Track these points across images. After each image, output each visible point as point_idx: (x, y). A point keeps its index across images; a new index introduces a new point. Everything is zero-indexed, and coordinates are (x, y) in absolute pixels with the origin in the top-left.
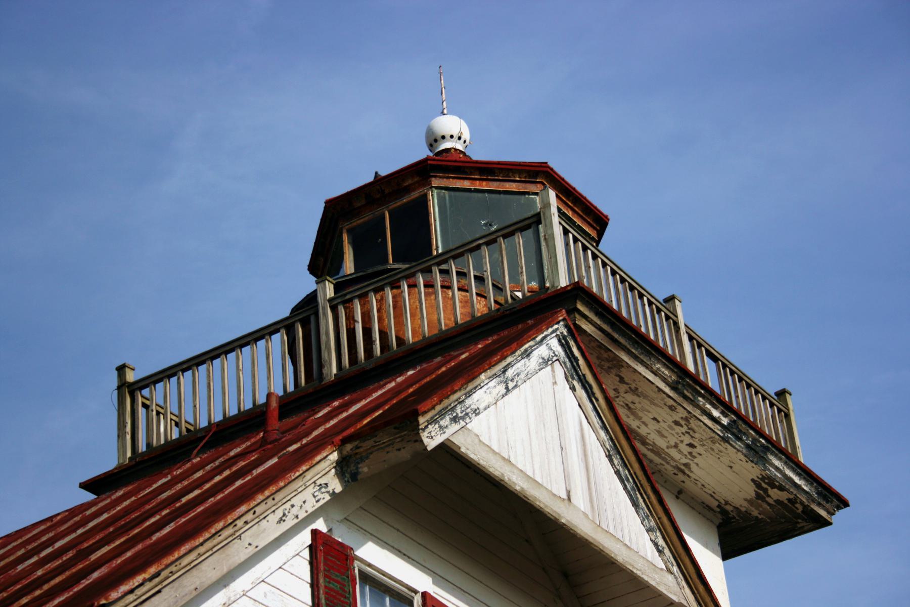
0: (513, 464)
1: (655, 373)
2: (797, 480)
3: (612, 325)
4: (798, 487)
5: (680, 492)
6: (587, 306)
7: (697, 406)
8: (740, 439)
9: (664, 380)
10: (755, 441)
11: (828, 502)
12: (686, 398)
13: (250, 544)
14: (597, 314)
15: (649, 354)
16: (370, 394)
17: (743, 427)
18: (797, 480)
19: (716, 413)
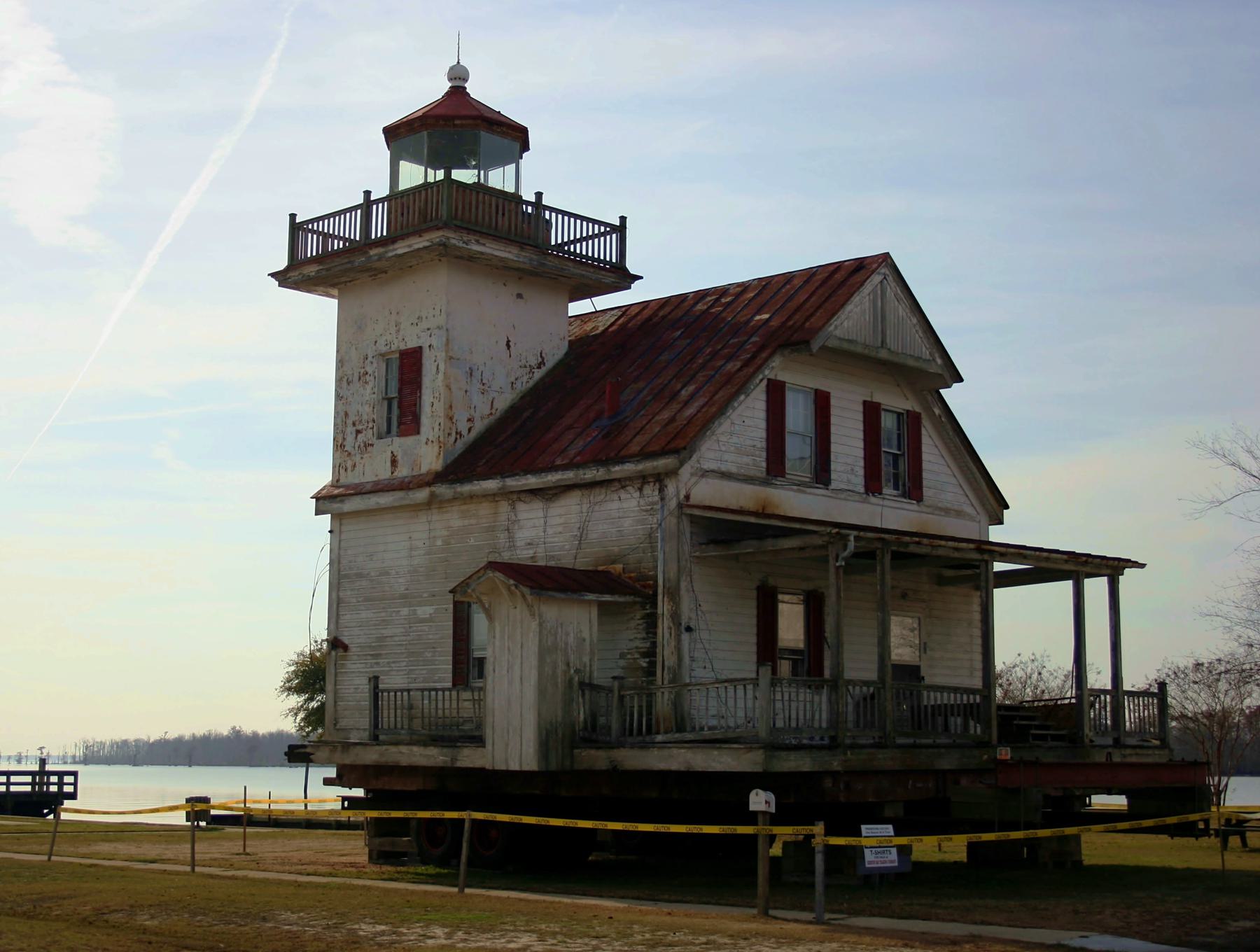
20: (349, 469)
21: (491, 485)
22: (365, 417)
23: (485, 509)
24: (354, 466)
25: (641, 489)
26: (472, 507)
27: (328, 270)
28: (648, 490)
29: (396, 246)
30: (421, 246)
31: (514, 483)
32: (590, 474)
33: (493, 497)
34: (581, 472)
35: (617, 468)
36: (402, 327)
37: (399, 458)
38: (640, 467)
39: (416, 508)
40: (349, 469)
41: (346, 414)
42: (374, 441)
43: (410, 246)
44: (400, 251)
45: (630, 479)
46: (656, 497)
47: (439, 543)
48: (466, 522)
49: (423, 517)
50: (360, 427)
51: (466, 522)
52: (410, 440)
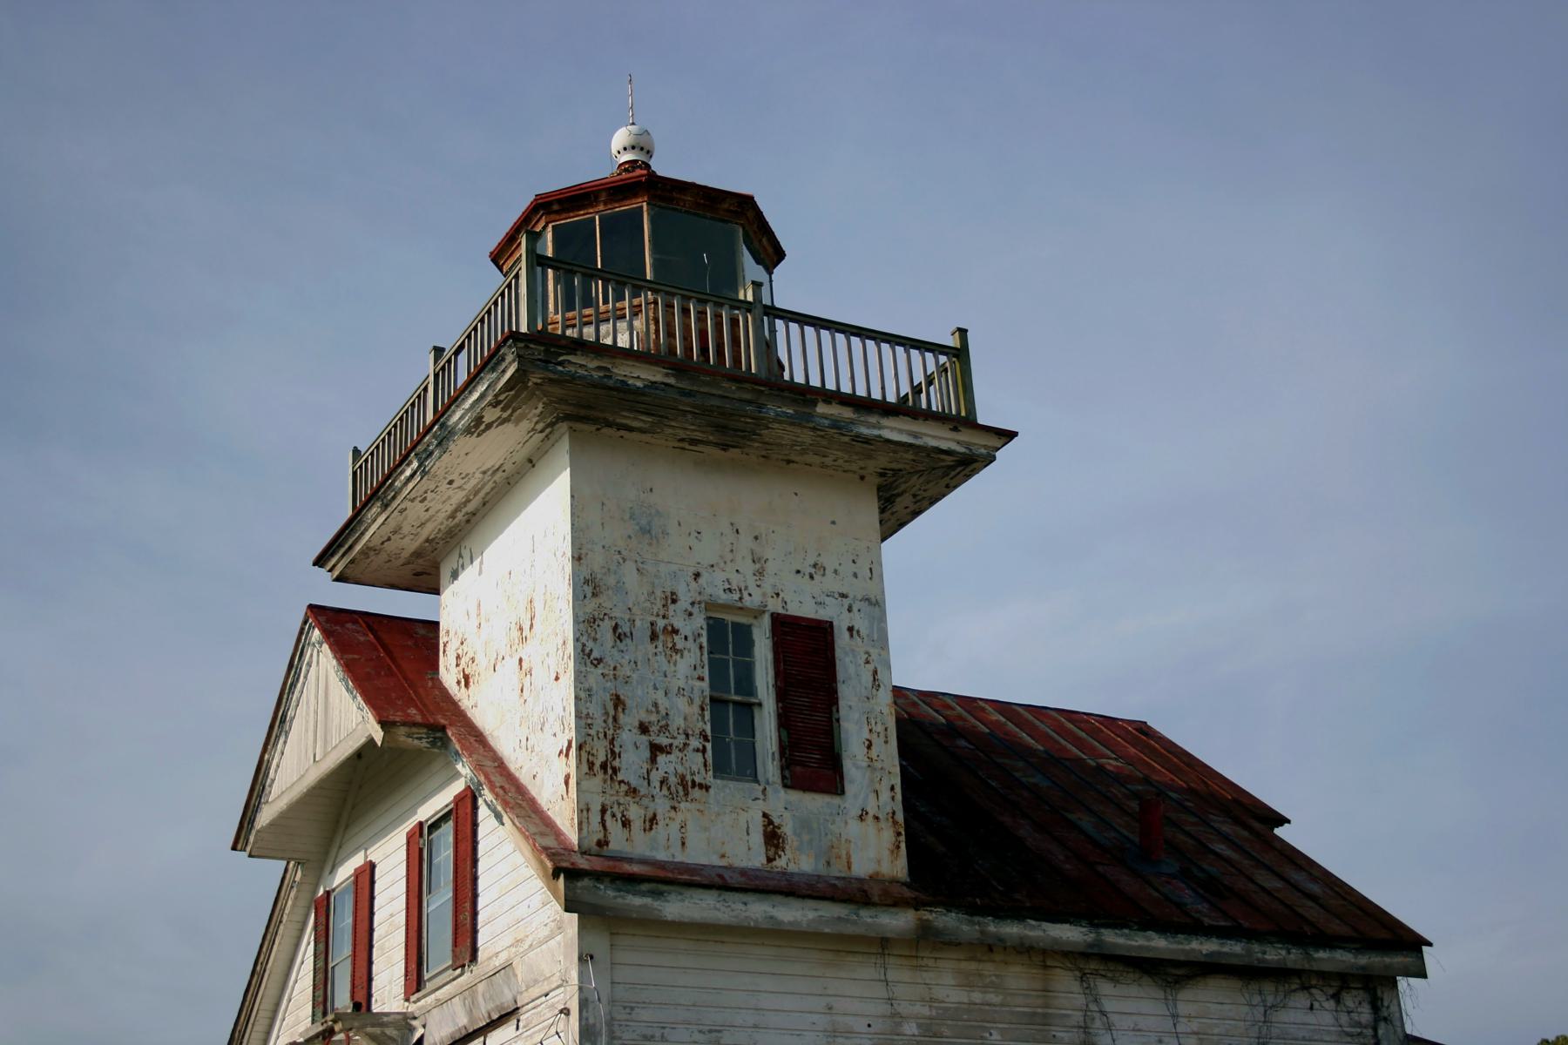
0: (327, 853)
1: (374, 521)
2: (476, 395)
3: (341, 546)
4: (482, 396)
5: (530, 461)
6: (625, 198)
7: (401, 489)
8: (431, 453)
9: (379, 514)
10: (435, 437)
11: (503, 360)
12: (394, 498)
13: (855, 575)
14: (332, 555)
15: (360, 522)
16: (413, 810)
17: (420, 448)
18: (476, 395)
19: (408, 472)
20: (637, 825)
21: (1070, 934)
22: (677, 722)
23: (1018, 978)
24: (653, 820)
25: (1336, 997)
26: (988, 969)
27: (683, 392)
28: (1349, 1000)
29: (885, 422)
30: (944, 445)
31: (1121, 941)
32: (1274, 954)
33: (1076, 958)
34: (1256, 947)
35: (1321, 954)
36: (771, 567)
37: (787, 829)
38: (1363, 960)
39: (883, 945)
40: (637, 825)
41: (618, 702)
42: (709, 778)
43: (915, 435)
44: (887, 434)
45: (1324, 976)
46: (1365, 1015)
47: (910, 1028)
48: (977, 996)
49: (899, 973)
50: (663, 740)
51: (977, 996)
52: (814, 802)
